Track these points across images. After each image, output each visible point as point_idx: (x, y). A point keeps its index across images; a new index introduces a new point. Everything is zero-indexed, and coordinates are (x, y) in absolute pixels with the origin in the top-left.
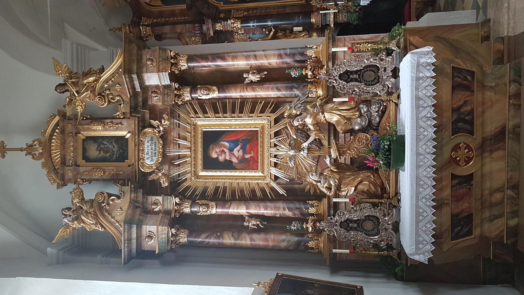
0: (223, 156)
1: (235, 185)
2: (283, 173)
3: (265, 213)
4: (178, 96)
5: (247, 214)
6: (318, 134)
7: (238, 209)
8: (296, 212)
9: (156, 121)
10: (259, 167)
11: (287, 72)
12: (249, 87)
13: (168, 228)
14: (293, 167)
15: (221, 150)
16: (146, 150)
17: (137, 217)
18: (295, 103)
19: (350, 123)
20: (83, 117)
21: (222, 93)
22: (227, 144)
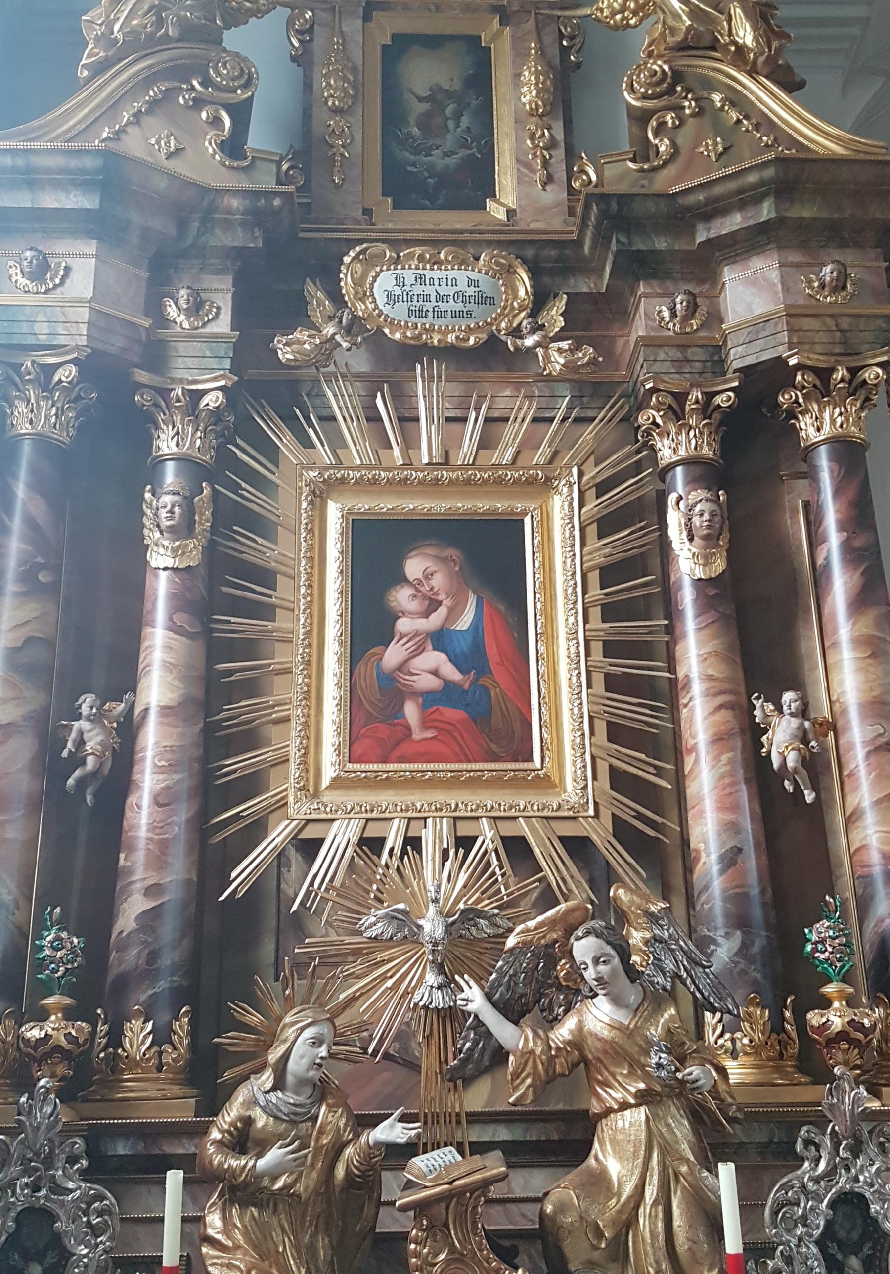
0: (413, 606)
1: (281, 657)
2: (332, 880)
3: (141, 797)
4: (675, 405)
5: (138, 710)
6: (529, 1069)
7: (167, 667)
8: (134, 952)
9: (561, 319)
10: (363, 767)
11: (827, 903)
12: (735, 716)
13: (77, 348)
14: (360, 933)
15: (440, 598)
16: (436, 274)
17: (135, 217)
18: (677, 944)
19: (596, 1255)
20: (571, 38)
21: (696, 600)
22: (465, 622)
